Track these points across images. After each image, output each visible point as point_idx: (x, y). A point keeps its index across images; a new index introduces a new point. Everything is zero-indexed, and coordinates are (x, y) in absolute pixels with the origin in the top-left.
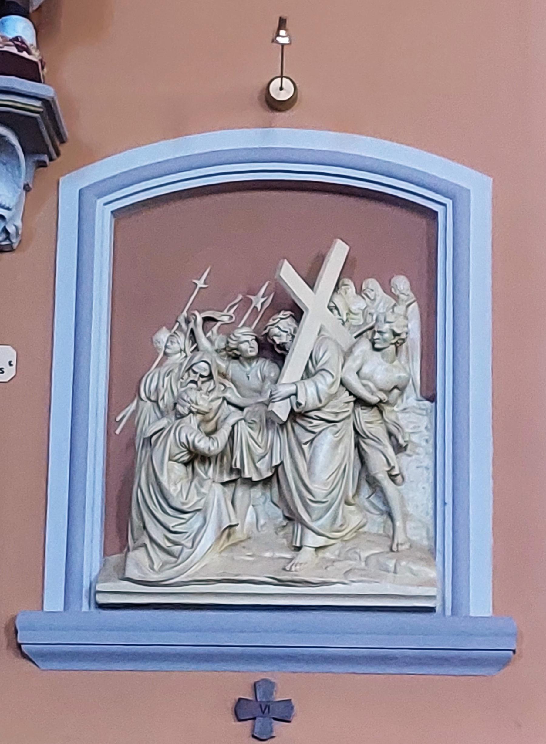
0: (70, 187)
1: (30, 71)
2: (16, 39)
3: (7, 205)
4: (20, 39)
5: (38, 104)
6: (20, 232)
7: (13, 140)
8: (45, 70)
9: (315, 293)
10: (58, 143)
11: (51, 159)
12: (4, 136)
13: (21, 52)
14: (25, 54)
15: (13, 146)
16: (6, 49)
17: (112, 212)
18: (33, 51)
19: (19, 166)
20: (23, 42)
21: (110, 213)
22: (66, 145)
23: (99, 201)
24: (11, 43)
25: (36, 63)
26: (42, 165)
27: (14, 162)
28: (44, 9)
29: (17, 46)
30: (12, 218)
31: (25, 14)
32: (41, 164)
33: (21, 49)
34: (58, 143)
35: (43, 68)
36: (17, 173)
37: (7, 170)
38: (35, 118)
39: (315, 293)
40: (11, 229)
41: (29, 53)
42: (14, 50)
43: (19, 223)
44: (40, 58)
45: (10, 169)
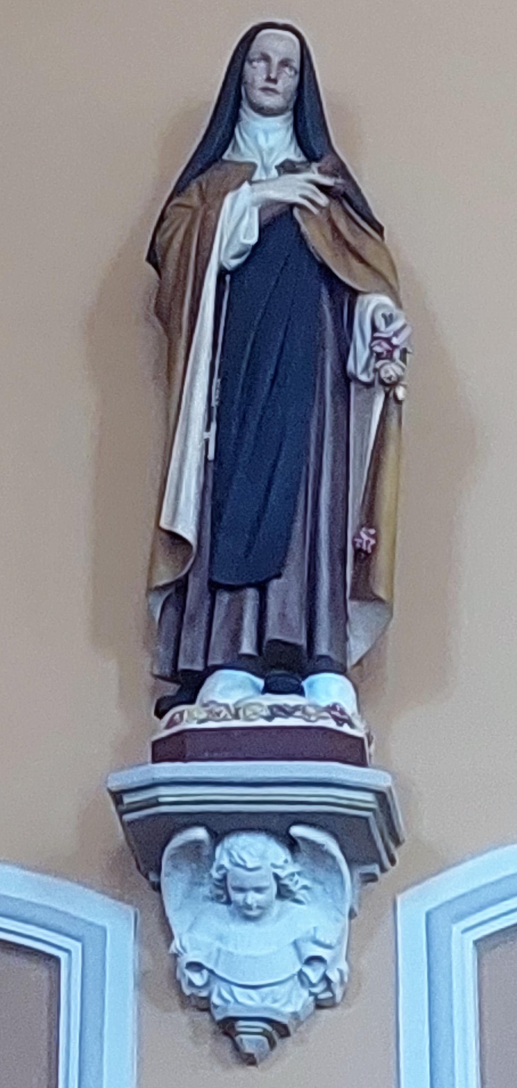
0: (411, 908)
1: (353, 751)
2: (333, 707)
3: (328, 942)
4: (338, 708)
5: (369, 797)
6: (346, 979)
7: (333, 847)
8: (373, 746)
9: (268, 84)
10: (392, 846)
11: (383, 869)
12: (323, 845)
13: (341, 725)
14: (346, 728)
15: (333, 858)
16: (321, 723)
17: (476, 943)
18: (356, 722)
19: (342, 883)
20: (342, 712)
21: (471, 945)
22: (402, 848)
23: (456, 929)
24: (325, 714)
25: (361, 740)
26: (372, 878)
27: (336, 879)
28: (365, 662)
29: (336, 719)
30: (335, 960)
31: (342, 671)
32: (368, 878)
33: (340, 722)
34: (392, 846)
35: (370, 743)
36: (338, 892)
37: (325, 890)
38: (366, 819)
39: (268, 84)
40: (334, 976)
41: (352, 725)
42: (331, 724)
43: (344, 966)
44: (367, 731)
45: (328, 890)
